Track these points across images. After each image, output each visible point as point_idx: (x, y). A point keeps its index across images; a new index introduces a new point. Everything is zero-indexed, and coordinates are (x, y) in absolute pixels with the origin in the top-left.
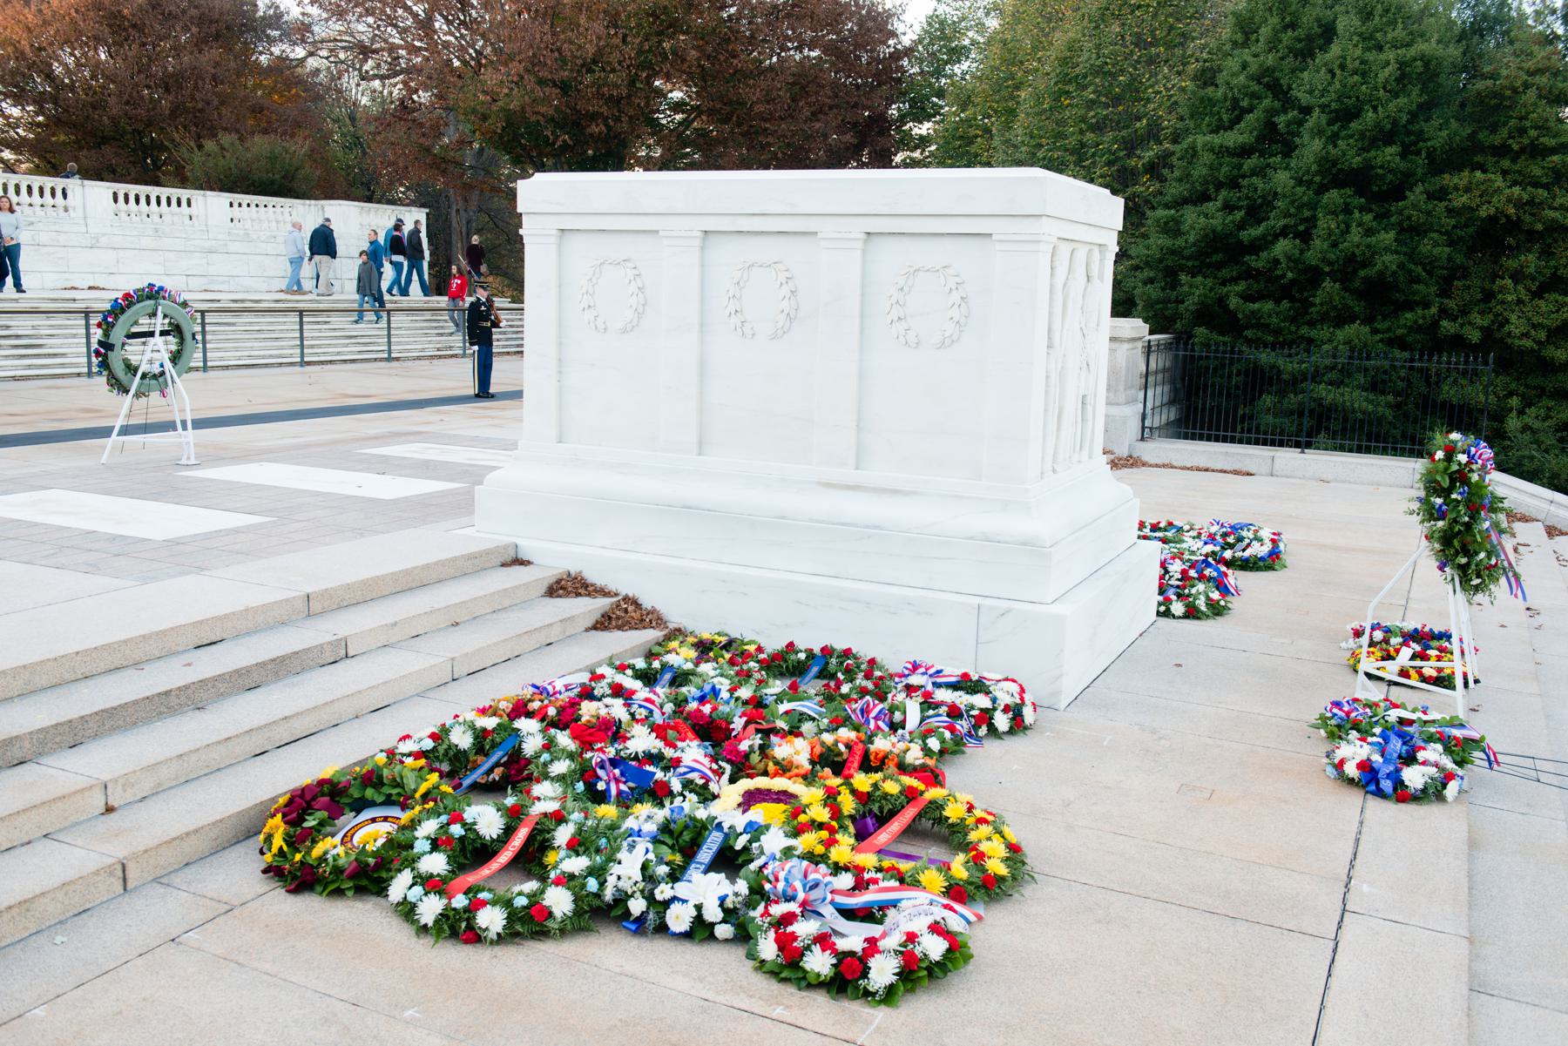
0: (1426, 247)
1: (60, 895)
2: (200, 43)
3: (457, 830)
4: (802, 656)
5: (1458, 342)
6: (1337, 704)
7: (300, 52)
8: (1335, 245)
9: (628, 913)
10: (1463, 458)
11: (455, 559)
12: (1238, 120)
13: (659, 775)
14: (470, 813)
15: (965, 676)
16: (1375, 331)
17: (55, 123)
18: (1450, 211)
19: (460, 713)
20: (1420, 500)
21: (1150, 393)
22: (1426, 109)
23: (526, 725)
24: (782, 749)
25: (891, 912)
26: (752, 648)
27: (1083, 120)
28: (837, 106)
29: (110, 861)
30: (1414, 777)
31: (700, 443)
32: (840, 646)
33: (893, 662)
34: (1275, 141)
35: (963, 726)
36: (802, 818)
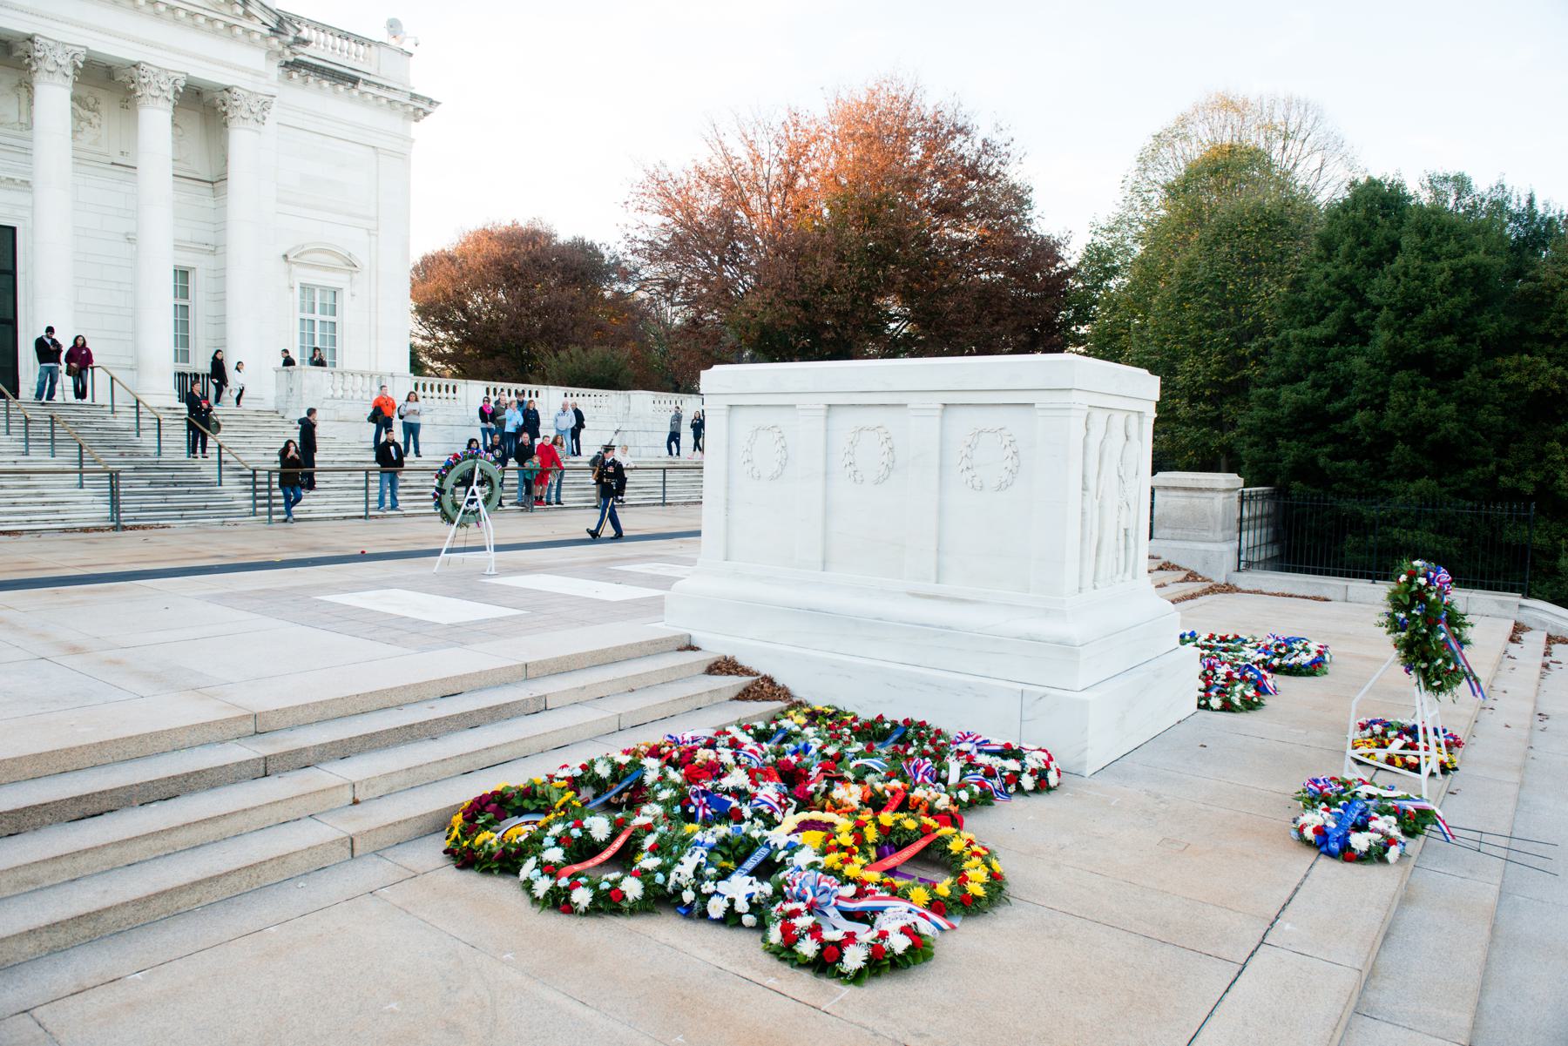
0: (1482, 416)
1: (306, 855)
2: (563, 284)
3: (576, 833)
4: (888, 726)
5: (1515, 494)
6: (1315, 781)
7: (632, 289)
8: (1405, 414)
9: (682, 902)
10: (1423, 581)
11: (640, 644)
12: (1322, 317)
13: (735, 803)
14: (588, 822)
15: (1008, 745)
16: (1442, 485)
17: (467, 341)
18: (1503, 387)
19: (606, 754)
20: (1389, 615)
21: (1244, 535)
22: (1478, 307)
23: (652, 764)
24: (839, 792)
25: (880, 917)
26: (849, 718)
27: (1200, 319)
28: (1015, 314)
29: (342, 835)
30: (1360, 841)
31: (824, 562)
32: (918, 719)
33: (952, 729)
34: (1355, 333)
35: (995, 784)
36: (832, 842)
